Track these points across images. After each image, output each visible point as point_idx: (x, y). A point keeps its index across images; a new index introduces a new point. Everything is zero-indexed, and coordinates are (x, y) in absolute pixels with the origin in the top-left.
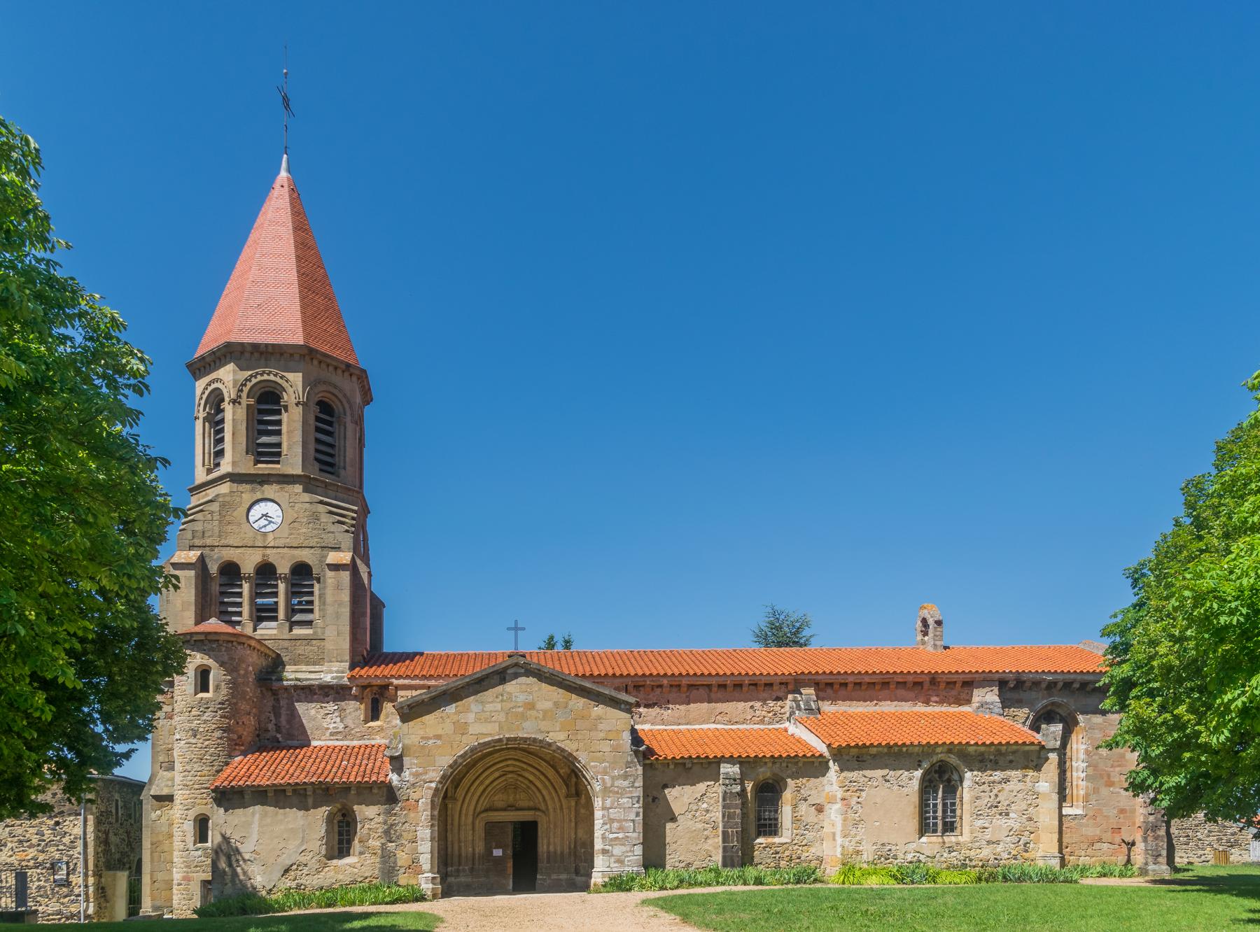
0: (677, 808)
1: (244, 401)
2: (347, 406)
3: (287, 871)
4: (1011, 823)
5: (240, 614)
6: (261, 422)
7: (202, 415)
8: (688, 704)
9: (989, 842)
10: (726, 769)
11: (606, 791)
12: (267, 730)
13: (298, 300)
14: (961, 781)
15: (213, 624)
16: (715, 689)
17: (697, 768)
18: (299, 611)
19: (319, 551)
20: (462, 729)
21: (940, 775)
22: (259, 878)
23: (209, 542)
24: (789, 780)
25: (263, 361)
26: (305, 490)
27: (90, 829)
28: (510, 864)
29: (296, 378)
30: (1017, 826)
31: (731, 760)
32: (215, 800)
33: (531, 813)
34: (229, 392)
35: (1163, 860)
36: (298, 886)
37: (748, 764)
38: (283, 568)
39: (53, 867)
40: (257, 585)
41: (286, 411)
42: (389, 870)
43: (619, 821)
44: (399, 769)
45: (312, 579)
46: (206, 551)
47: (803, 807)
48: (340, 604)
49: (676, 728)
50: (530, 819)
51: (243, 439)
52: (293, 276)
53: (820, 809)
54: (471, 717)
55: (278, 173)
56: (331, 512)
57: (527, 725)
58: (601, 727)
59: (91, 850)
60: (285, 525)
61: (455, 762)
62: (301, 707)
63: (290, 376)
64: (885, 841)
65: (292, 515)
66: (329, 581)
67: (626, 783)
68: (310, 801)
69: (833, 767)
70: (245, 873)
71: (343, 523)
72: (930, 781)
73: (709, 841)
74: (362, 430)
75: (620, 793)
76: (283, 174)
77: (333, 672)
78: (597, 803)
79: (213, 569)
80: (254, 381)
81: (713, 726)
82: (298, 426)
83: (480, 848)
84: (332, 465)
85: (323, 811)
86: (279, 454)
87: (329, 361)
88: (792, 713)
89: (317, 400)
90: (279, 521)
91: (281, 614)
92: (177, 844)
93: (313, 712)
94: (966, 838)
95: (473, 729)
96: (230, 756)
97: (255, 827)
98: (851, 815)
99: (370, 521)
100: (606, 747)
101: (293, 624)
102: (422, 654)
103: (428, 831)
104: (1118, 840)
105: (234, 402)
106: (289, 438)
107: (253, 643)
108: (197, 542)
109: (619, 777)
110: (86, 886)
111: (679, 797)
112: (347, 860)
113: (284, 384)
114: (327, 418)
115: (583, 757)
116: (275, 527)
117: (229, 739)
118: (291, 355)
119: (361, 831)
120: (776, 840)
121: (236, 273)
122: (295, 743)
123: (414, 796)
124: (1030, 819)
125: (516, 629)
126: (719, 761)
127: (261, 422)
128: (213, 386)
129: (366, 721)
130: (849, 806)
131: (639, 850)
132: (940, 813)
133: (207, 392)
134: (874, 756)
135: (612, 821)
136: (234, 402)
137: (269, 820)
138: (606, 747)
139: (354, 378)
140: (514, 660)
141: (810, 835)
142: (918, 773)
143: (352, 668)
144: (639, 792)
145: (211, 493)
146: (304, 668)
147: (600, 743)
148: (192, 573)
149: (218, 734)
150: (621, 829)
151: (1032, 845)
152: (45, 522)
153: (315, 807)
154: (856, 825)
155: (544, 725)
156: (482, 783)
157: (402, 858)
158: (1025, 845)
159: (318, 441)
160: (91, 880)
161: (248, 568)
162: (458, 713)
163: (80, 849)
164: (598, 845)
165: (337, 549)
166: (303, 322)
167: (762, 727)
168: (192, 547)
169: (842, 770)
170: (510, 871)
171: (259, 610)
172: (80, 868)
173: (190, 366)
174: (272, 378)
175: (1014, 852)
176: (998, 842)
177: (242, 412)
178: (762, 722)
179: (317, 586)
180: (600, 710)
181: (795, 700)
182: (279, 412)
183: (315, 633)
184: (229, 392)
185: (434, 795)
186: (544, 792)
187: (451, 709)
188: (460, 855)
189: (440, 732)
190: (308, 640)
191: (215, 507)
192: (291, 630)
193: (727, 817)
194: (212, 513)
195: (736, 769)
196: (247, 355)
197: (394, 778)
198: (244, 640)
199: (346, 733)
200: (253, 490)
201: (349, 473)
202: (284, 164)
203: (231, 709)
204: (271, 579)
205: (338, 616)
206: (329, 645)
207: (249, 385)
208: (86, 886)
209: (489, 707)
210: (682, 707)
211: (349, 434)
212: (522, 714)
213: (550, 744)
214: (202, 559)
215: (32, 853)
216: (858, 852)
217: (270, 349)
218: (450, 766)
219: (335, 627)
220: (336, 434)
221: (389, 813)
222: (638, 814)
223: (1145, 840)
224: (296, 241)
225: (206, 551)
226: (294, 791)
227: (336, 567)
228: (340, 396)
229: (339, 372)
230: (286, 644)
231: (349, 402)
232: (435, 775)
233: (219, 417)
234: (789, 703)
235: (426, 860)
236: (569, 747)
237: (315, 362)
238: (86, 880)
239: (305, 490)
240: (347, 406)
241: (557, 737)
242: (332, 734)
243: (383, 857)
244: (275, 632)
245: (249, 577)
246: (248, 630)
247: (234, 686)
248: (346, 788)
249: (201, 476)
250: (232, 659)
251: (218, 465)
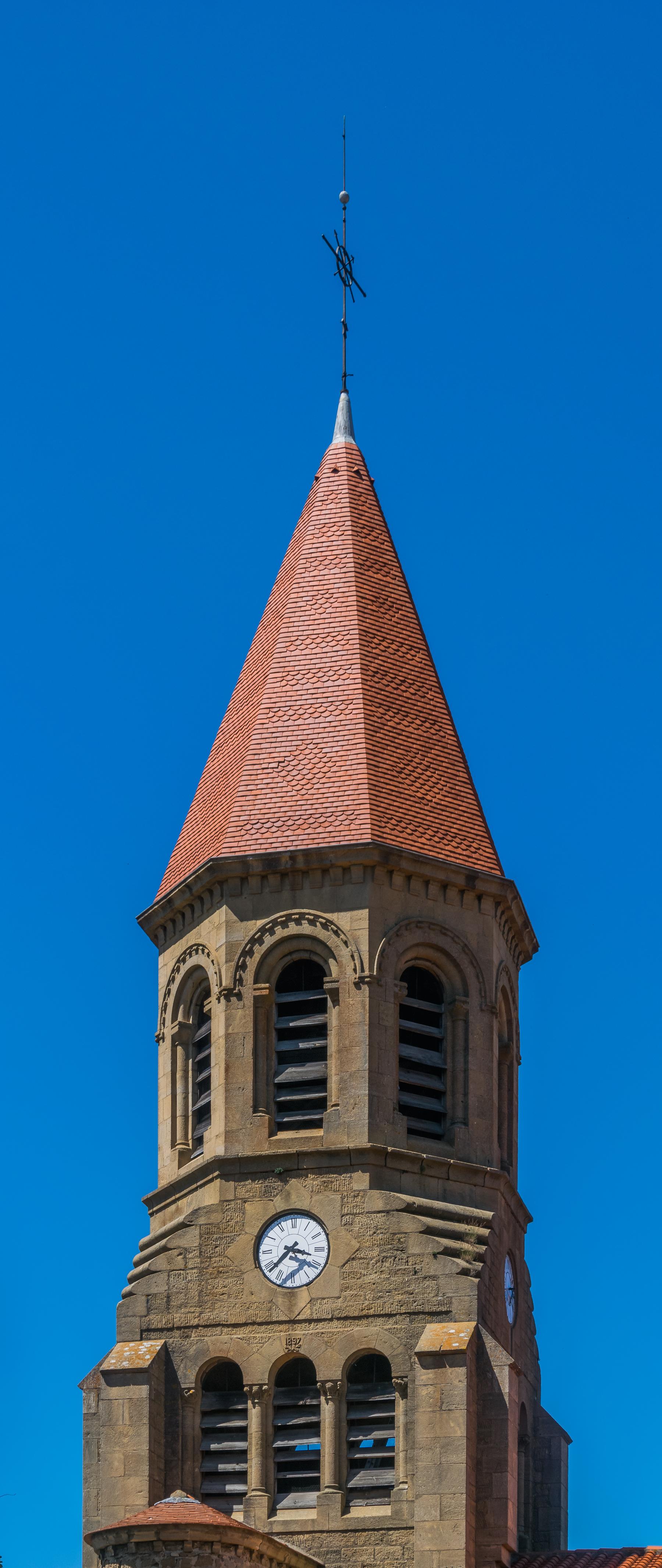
1: (249, 991)
5: (242, 1477)
6: (285, 1034)
7: (169, 1030)
13: (361, 737)
18: (364, 1464)
19: (403, 1324)
23: (178, 1317)
25: (286, 894)
29: (355, 923)
34: (219, 974)
38: (330, 1368)
40: (279, 1410)
41: (336, 1002)
46: (174, 1339)
48: (447, 1445)
51: (246, 1079)
52: (352, 681)
55: (330, 440)
56: (430, 1231)
60: (334, 1269)
63: (342, 919)
65: (348, 1242)
66: (423, 1392)
74: (512, 1024)
76: (340, 439)
79: (188, 1377)
80: (269, 940)
82: (361, 1034)
84: (437, 1117)
87: (427, 871)
89: (403, 966)
99: (533, 1240)
102: (641, 1552)
105: (228, 994)
106: (342, 1064)
107: (257, 1544)
108: (157, 1320)
113: (332, 940)
114: (425, 1005)
116: (312, 1273)
118: (346, 870)
121: (239, 693)
127: (285, 1034)
128: (191, 962)
133: (179, 978)
136: (228, 994)
139: (488, 905)
145: (187, 1205)
148: (143, 1391)
159: (405, 1063)
161: (258, 1371)
165: (442, 1315)
166: (372, 787)
168: (146, 1333)
171: (282, 1467)
174: (306, 929)
177: (244, 1014)
179: (401, 1406)
182: (320, 1007)
183: (396, 1513)
190: (380, 1529)
191: (190, 1239)
192: (346, 1509)
196: (254, 882)
198: (235, 1538)
201: (476, 1133)
202: (341, 418)
204: (304, 1394)
207: (259, 951)
214: (165, 1357)
217: (301, 864)
219: (433, 1500)
220: (447, 1045)
224: (361, 598)
225: (174, 1339)
227: (437, 1359)
228: (455, 950)
229: (452, 893)
230: (336, 1541)
231: (474, 962)
233: (202, 1032)
237: (398, 879)
239: (376, 1184)
240: (469, 971)
244: (312, 1515)
245: (260, 1394)
246: (251, 1514)
249: (169, 1170)
251: (199, 1141)
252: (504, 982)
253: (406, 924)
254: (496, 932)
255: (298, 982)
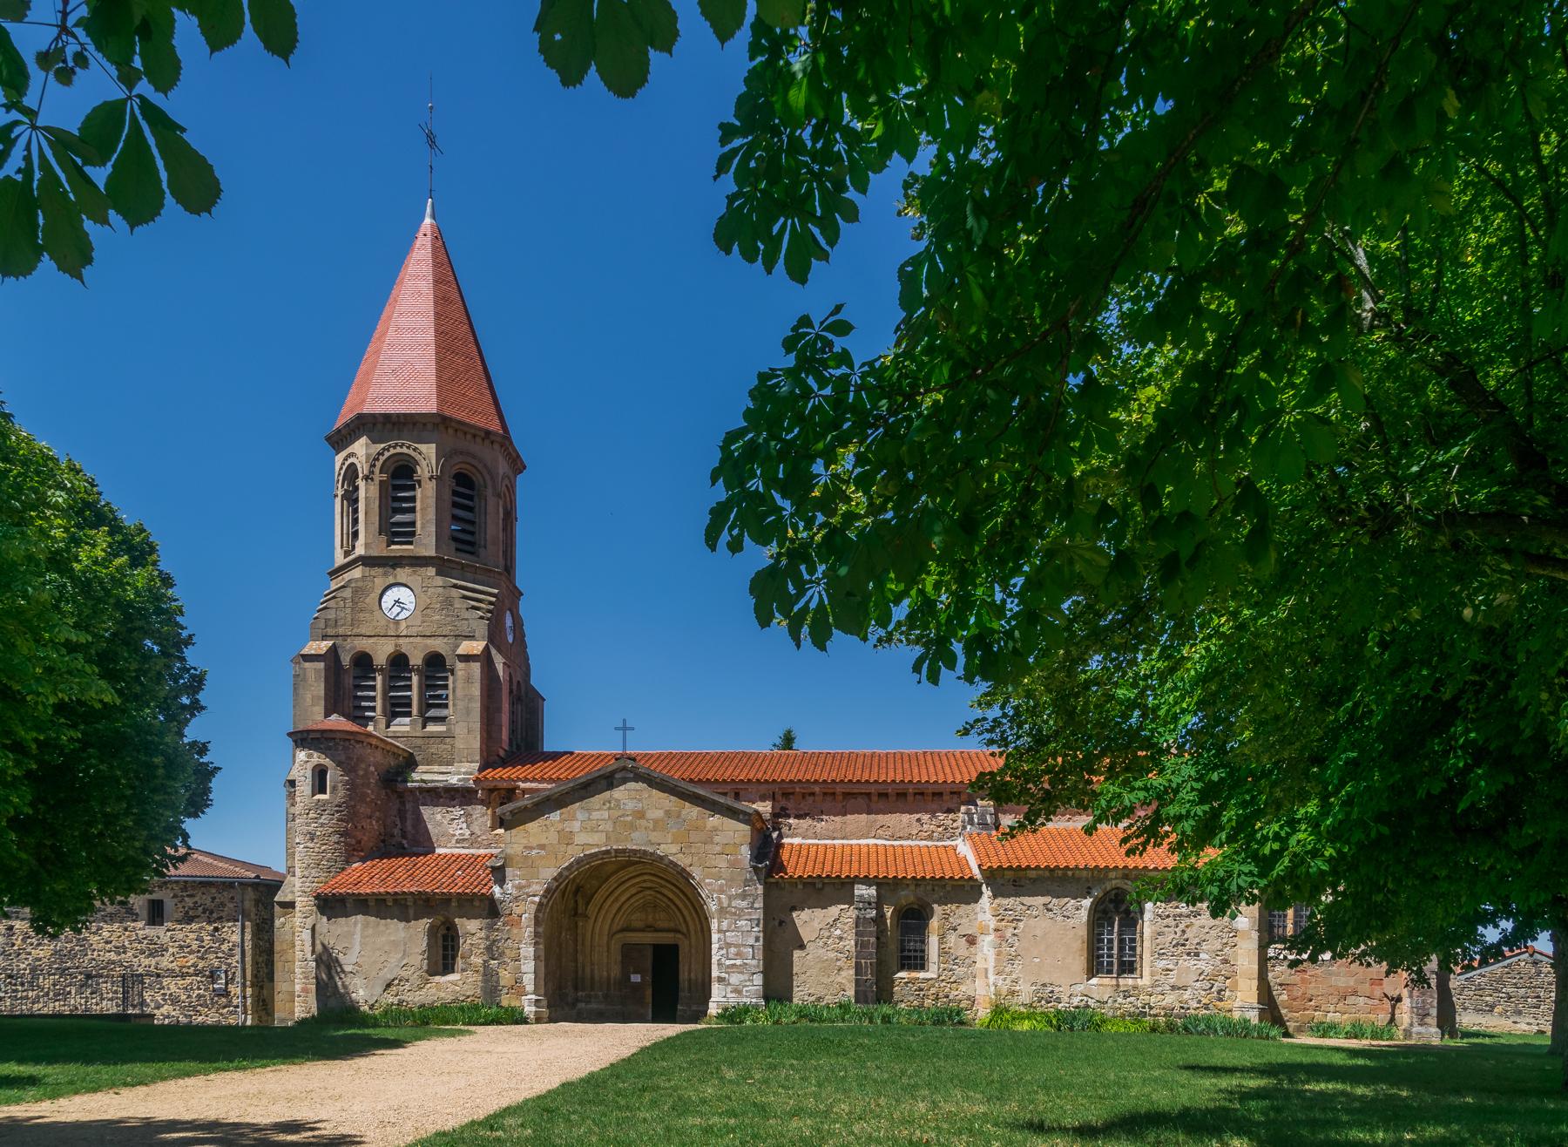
0: (806, 934)
1: (377, 477)
2: (487, 477)
3: (389, 986)
4: (1202, 965)
7: (340, 492)
8: (844, 814)
9: (1173, 988)
10: (862, 891)
11: (722, 911)
12: (392, 836)
14: (1142, 912)
15: (337, 722)
16: (875, 798)
17: (829, 889)
18: (433, 702)
19: (452, 640)
20: (567, 838)
21: (1115, 909)
22: (361, 992)
23: (341, 631)
24: (935, 906)
26: (438, 574)
27: (248, 936)
28: (649, 992)
29: (429, 450)
30: (1209, 969)
31: (867, 881)
32: (318, 907)
33: (671, 935)
34: (363, 469)
35: (1432, 1020)
36: (400, 1003)
37: (888, 887)
38: (416, 659)
39: (213, 976)
40: (392, 678)
42: (491, 987)
43: (736, 946)
44: (501, 881)
45: (445, 670)
46: (339, 641)
47: (952, 938)
48: (471, 699)
49: (809, 842)
50: (671, 942)
52: (430, 336)
53: (972, 941)
54: (576, 826)
57: (635, 835)
58: (717, 839)
59: (248, 959)
61: (560, 874)
62: (426, 812)
63: (423, 447)
64: (1047, 981)
67: (744, 904)
68: (411, 912)
69: (987, 892)
70: (345, 987)
71: (478, 609)
72: (1105, 912)
73: (843, 973)
75: (738, 915)
76: (428, 220)
77: (460, 773)
78: (714, 925)
79: (346, 660)
80: (387, 454)
81: (872, 841)
83: (616, 971)
85: (425, 923)
86: (413, 534)
88: (964, 828)
89: (454, 472)
90: (412, 607)
91: (415, 710)
92: (299, 955)
93: (439, 817)
94: (1145, 981)
95: (581, 839)
96: (348, 862)
97: (357, 937)
98: (1005, 949)
100: (722, 862)
101: (426, 721)
103: (532, 949)
104: (1378, 993)
105: (366, 478)
106: (422, 516)
108: (330, 631)
109: (737, 896)
110: (244, 997)
111: (809, 921)
112: (451, 977)
113: (418, 457)
114: (463, 490)
115: (696, 873)
117: (346, 844)
119: (464, 946)
120: (922, 975)
122: (421, 850)
123: (517, 911)
124: (1226, 961)
125: (625, 729)
126: (852, 881)
129: (493, 828)
130: (1002, 938)
131: (758, 980)
132: (1115, 951)
134: (1034, 881)
135: (729, 945)
136: (366, 478)
137: (370, 931)
138: (722, 862)
140: (621, 763)
141: (960, 971)
142: (1087, 902)
143: (481, 770)
144: (759, 914)
146: (436, 768)
147: (715, 856)
148: (322, 665)
149: (335, 838)
150: (739, 955)
151: (1227, 993)
152: (835, 494)
153: (416, 919)
154: (1011, 960)
155: (654, 837)
156: (617, 899)
157: (505, 977)
158: (1219, 992)
160: (249, 991)
161: (380, 659)
162: (563, 821)
163: (238, 957)
164: (715, 973)
165: (471, 637)
167: (930, 843)
168: (325, 637)
169: (995, 896)
170: (649, 999)
172: (238, 979)
173: (328, 439)
174: (405, 450)
175: (1205, 1001)
176: (1185, 988)
177: (374, 489)
178: (930, 838)
180: (715, 820)
181: (968, 813)
182: (413, 488)
184: (363, 469)
185: (538, 910)
186: (686, 913)
187: (555, 816)
188: (592, 978)
189: (544, 841)
190: (441, 737)
191: (347, 593)
193: (861, 945)
194: (344, 599)
195: (873, 891)
196: (379, 426)
197: (497, 889)
199: (473, 841)
200: (385, 574)
202: (429, 210)
203: (349, 813)
205: (468, 711)
206: (459, 744)
207: (382, 459)
208: (244, 997)
209: (596, 815)
210: (837, 819)
211: (490, 509)
212: (631, 823)
213: (661, 858)
214: (334, 650)
215: (192, 959)
216: (1013, 993)
218: (555, 879)
221: (490, 928)
222: (757, 939)
223: (1411, 996)
225: (339, 641)
226: (395, 901)
227: (466, 658)
228: (480, 467)
229: (479, 440)
230: (419, 742)
231: (489, 472)
232: (538, 888)
234: (961, 816)
235: (529, 981)
236: (683, 861)
237: (451, 431)
238: (244, 991)
239: (438, 574)
240: (487, 477)
241: (669, 850)
242: (458, 841)
243: (485, 975)
245: (382, 670)
247: (352, 787)
248: (446, 900)
249: (340, 559)
250: (350, 759)
252: (506, 482)
253: (455, 452)
254: (501, 459)
255: (400, 475)
